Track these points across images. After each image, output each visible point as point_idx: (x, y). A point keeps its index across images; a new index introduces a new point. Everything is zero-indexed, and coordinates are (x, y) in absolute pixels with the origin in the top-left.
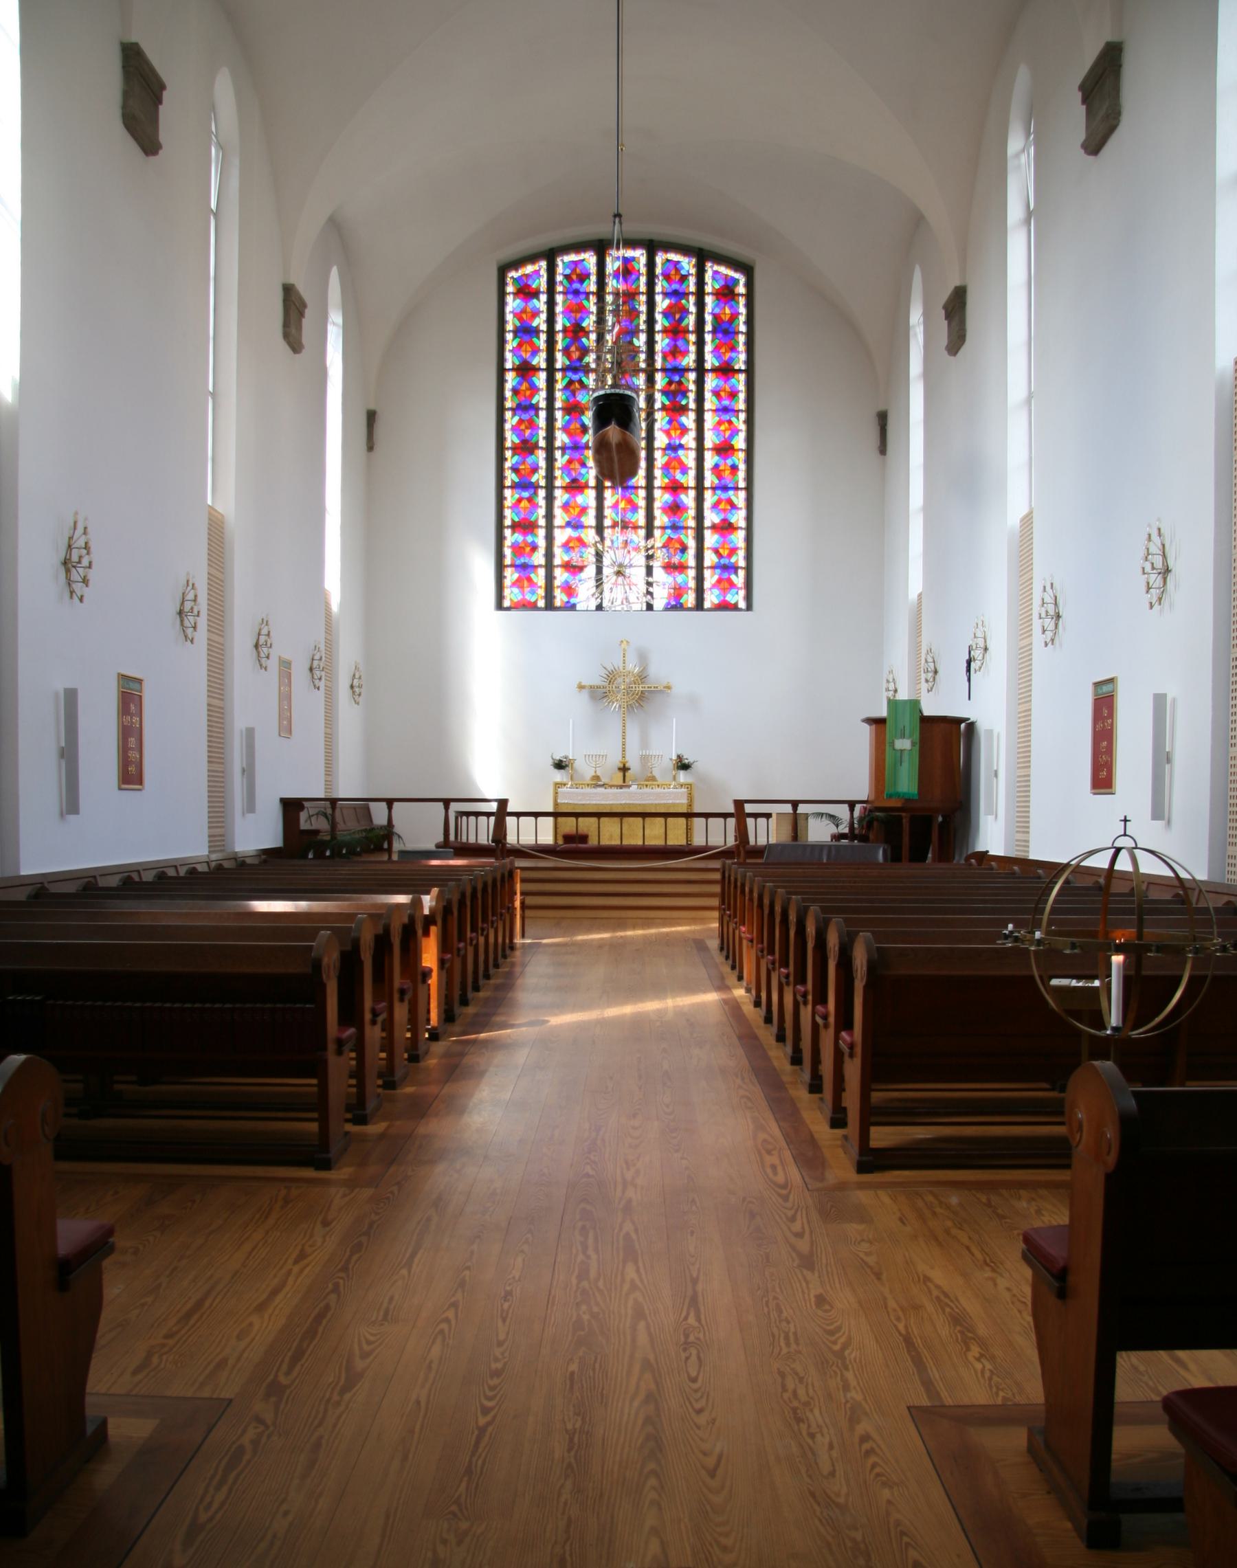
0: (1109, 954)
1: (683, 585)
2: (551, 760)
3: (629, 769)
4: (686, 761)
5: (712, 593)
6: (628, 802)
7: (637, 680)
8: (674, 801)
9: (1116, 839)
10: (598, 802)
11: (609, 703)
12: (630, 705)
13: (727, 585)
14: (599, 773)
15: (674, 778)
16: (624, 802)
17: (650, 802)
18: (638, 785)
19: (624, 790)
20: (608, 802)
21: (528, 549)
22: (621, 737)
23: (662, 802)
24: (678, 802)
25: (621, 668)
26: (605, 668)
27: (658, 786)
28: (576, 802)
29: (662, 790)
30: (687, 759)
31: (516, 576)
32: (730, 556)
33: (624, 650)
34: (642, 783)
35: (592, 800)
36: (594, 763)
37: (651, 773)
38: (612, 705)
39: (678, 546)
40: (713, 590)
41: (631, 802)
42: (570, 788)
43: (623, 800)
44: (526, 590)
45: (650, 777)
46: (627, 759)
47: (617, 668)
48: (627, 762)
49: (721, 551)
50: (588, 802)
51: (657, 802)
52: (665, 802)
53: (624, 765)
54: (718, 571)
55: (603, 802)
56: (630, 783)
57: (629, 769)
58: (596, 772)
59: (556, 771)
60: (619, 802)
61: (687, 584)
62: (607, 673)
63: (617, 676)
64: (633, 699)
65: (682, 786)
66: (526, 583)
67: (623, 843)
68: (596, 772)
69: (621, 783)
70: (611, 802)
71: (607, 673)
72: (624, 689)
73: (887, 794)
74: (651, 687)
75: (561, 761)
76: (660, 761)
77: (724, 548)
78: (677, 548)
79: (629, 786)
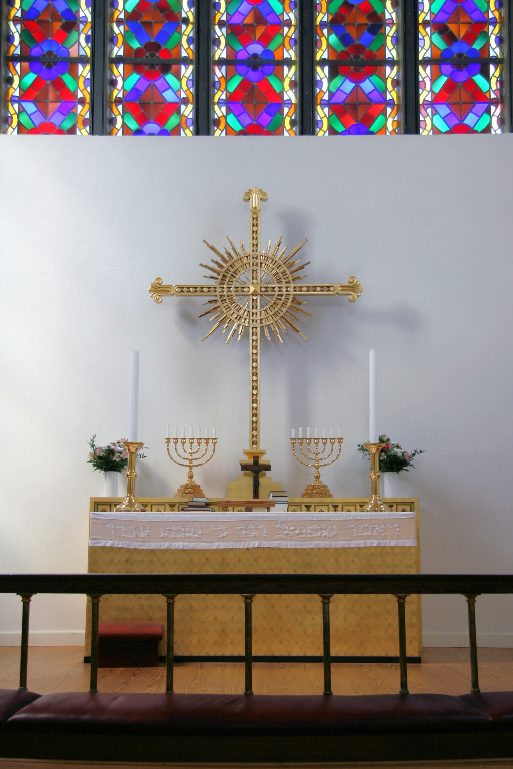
0: (392, 457)
1: (375, 97)
2: (91, 450)
3: (268, 468)
4: (399, 452)
5: (435, 112)
6: (265, 544)
7: (284, 272)
8: (384, 542)
9: (177, 452)
10: (191, 546)
11: (222, 322)
12: (269, 326)
13: (465, 95)
14: (197, 480)
15: (375, 490)
16: (256, 544)
17: (323, 544)
18: (290, 504)
19: (258, 514)
20: (214, 546)
21: (58, 26)
22: (249, 399)
23: (353, 544)
24: (393, 543)
25: (249, 250)
26: (213, 248)
27: (335, 507)
28: (134, 545)
29: (345, 514)
30: (398, 447)
31: (31, 78)
32: (470, 38)
33: (255, 211)
34: (298, 500)
35: (175, 539)
36: (188, 456)
37: (317, 477)
38: (228, 328)
39: (363, 20)
40: (438, 107)
41: (274, 544)
42: (126, 510)
43: (255, 538)
44: (53, 106)
45: (314, 487)
46: (262, 446)
47: (239, 250)
48: (263, 453)
49: (452, 27)
50: (165, 546)
51: (340, 544)
52: (362, 543)
53: (256, 459)
54: (447, 68)
55: (202, 546)
56: (271, 498)
57: (268, 468)
58: (191, 477)
59: (100, 473)
60: (242, 545)
61: (383, 94)
62: (219, 260)
63: (237, 266)
64: (275, 314)
65: (391, 506)
66: (52, 93)
67: (177, 690)
68: (191, 477)
69: (248, 496)
70: (223, 545)
71: (219, 260)
72: (255, 294)
73: (127, 466)
74: (314, 288)
75: (110, 452)
76: (335, 453)
77: (456, 22)
78: (360, 25)
79: (268, 506)
